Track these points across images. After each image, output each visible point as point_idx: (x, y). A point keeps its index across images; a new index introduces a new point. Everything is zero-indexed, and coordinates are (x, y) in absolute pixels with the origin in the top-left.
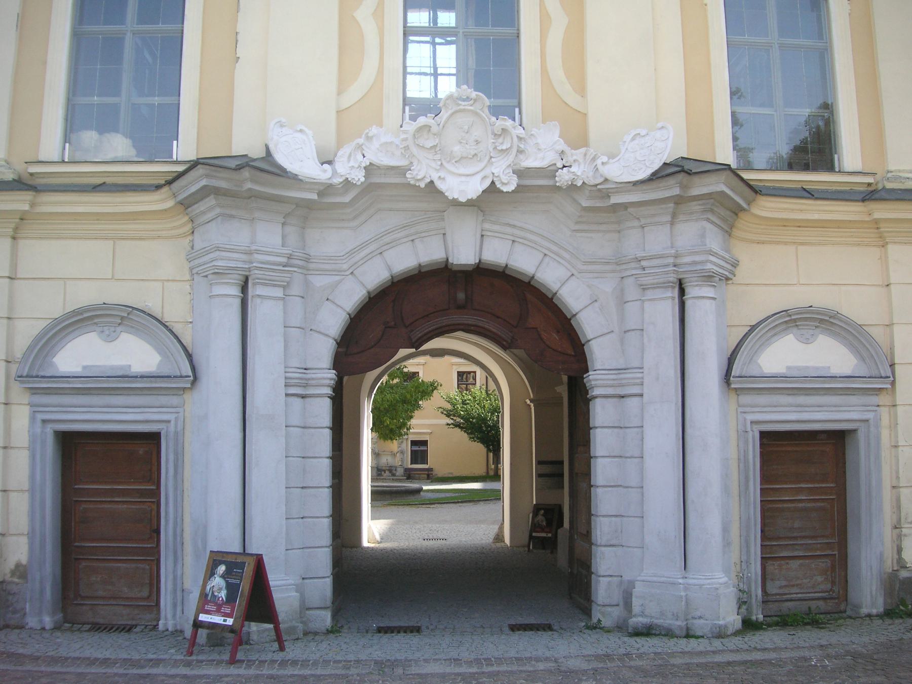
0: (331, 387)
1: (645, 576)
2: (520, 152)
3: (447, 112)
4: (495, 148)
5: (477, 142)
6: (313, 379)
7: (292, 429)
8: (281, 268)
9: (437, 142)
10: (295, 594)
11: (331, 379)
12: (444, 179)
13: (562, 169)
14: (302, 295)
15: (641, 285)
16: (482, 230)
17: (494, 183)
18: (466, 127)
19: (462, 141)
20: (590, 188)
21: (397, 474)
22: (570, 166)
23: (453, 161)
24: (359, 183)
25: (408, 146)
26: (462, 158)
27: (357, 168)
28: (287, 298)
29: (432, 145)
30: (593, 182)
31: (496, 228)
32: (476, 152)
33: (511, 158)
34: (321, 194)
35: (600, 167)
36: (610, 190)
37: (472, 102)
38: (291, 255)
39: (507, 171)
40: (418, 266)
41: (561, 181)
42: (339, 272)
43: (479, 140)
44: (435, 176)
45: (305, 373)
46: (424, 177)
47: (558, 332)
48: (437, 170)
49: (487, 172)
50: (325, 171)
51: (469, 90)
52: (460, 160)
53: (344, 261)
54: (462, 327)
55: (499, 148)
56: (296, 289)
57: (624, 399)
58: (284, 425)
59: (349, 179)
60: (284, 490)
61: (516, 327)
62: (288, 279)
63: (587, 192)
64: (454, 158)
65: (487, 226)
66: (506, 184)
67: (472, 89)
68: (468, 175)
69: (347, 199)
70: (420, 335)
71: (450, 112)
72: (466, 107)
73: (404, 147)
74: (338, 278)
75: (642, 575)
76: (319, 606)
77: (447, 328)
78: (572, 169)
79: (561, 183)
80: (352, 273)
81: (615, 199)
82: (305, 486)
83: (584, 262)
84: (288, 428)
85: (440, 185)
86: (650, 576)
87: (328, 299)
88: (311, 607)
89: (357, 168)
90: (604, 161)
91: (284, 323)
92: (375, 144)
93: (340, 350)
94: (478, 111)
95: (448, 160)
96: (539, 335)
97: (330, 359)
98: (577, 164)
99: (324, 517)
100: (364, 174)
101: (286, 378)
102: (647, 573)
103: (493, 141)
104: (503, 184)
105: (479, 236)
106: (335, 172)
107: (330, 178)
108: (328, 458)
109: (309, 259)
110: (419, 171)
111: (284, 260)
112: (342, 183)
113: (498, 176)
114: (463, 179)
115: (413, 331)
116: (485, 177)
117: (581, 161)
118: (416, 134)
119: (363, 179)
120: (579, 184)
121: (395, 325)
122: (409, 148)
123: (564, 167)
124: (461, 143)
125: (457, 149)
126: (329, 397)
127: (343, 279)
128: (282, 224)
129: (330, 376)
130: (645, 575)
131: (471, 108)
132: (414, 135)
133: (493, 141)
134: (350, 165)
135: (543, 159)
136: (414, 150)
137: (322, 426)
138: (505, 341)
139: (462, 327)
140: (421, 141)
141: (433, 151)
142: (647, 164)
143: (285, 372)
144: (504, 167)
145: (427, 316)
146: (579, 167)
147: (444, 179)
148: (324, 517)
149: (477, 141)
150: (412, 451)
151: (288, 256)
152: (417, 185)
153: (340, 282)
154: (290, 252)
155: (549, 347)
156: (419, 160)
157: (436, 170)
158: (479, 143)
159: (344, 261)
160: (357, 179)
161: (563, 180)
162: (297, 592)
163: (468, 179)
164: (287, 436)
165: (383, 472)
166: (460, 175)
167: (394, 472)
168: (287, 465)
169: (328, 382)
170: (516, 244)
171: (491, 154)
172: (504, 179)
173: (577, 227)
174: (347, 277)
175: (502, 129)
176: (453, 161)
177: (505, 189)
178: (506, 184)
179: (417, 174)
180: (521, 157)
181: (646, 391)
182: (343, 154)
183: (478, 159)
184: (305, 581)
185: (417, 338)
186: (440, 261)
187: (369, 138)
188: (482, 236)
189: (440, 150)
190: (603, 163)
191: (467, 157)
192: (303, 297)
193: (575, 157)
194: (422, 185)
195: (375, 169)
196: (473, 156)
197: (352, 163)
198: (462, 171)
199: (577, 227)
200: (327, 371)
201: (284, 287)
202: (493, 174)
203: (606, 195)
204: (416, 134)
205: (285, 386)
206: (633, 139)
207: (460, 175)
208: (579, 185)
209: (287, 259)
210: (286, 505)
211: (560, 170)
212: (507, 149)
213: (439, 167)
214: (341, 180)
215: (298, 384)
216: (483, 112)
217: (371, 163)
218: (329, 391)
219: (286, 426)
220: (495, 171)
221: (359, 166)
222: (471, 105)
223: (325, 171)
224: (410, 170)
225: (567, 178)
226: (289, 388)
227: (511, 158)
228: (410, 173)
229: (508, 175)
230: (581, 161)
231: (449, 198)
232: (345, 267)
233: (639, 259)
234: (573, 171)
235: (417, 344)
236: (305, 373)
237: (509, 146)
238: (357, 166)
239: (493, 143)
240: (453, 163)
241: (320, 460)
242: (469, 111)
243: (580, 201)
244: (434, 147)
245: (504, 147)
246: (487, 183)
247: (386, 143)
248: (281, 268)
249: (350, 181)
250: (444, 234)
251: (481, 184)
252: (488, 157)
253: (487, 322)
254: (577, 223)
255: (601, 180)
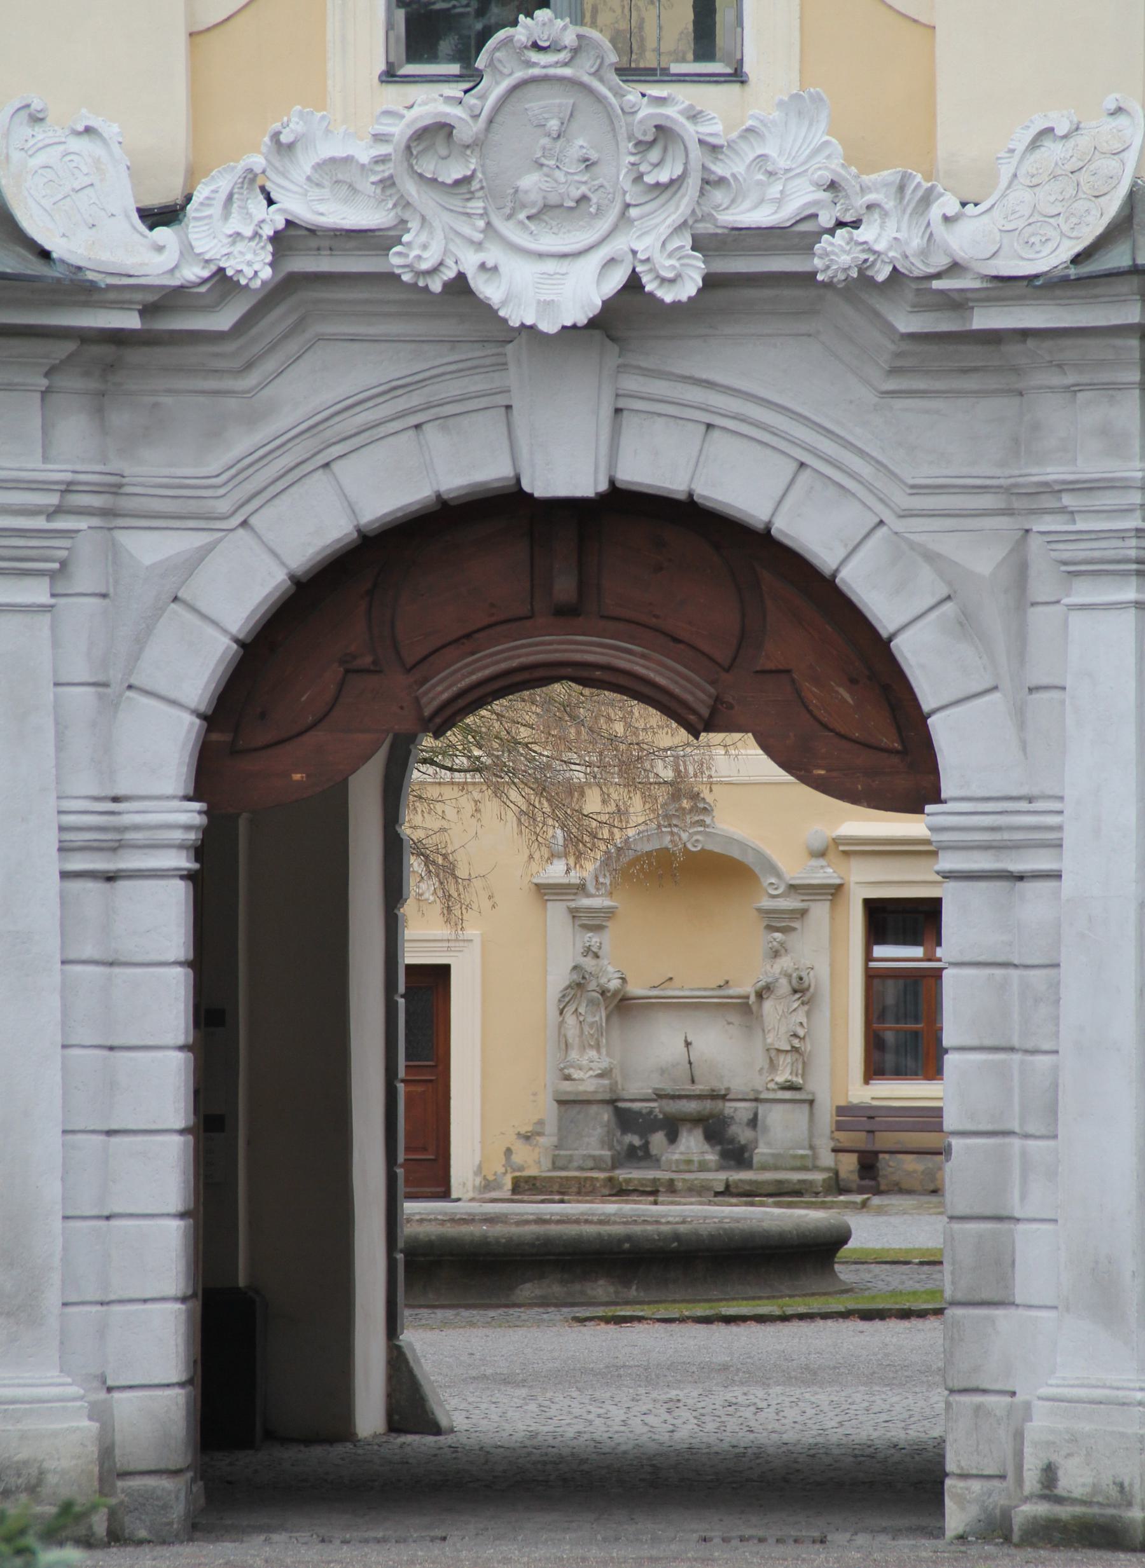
0: (187, 848)
1: (1058, 1386)
2: (710, 182)
3: (497, 83)
4: (639, 178)
5: (588, 164)
6: (137, 828)
7: (79, 968)
8: (40, 523)
9: (472, 167)
10: (86, 1423)
11: (188, 828)
12: (495, 269)
13: (831, 232)
14: (104, 591)
15: (1065, 563)
16: (617, 395)
17: (639, 279)
18: (553, 124)
19: (543, 161)
20: (914, 286)
21: (762, 1151)
22: (856, 224)
23: (522, 216)
24: (256, 284)
25: (391, 177)
26: (547, 208)
27: (251, 239)
28: (62, 601)
29: (459, 176)
30: (920, 268)
31: (659, 387)
32: (584, 189)
33: (680, 208)
34: (148, 311)
35: (938, 228)
36: (969, 295)
37: (563, 56)
38: (70, 483)
39: (676, 243)
40: (434, 498)
41: (828, 267)
42: (205, 519)
43: (594, 155)
44: (469, 262)
45: (112, 813)
46: (441, 264)
47: (853, 681)
48: (479, 246)
49: (620, 244)
50: (160, 249)
51: (559, 23)
52: (540, 212)
53: (222, 491)
54: (569, 671)
55: (649, 179)
56: (85, 578)
57: (1020, 885)
58: (57, 958)
59: (229, 272)
60: (57, 1139)
61: (727, 670)
62: (64, 554)
63: (910, 295)
64: (523, 206)
65: (631, 383)
66: (672, 281)
67: (568, 20)
68: (564, 256)
69: (223, 320)
70: (445, 696)
71: (505, 85)
72: (552, 71)
73: (381, 181)
74: (200, 539)
75: (1052, 1381)
76: (153, 1468)
77: (525, 676)
78: (861, 234)
79: (830, 273)
80: (244, 524)
81: (984, 319)
82: (115, 1127)
83: (913, 487)
84: (68, 967)
85: (489, 290)
86: (1072, 1386)
87: (175, 599)
88: (131, 1468)
89: (251, 239)
90: (950, 213)
91: (55, 671)
92: (305, 163)
93: (215, 737)
94: (586, 79)
95: (507, 211)
96: (798, 692)
97: (184, 769)
98: (876, 215)
99: (168, 1215)
100: (269, 258)
101: (62, 829)
102: (1064, 1378)
103: (632, 159)
104: (664, 281)
105: (606, 412)
106: (187, 250)
107: (172, 271)
108: (181, 1048)
109: (121, 486)
110: (425, 247)
111: (53, 499)
112: (205, 281)
113: (648, 260)
114: (551, 266)
115: (426, 680)
116: (612, 261)
117: (889, 205)
118: (413, 144)
119: (266, 273)
120: (882, 274)
121: (374, 663)
122: (394, 184)
123: (840, 224)
124: (542, 165)
125: (530, 181)
126: (182, 877)
127: (219, 541)
128: (42, 392)
129: (183, 818)
130: (1059, 1382)
131: (567, 72)
132: (408, 148)
133: (632, 159)
134: (230, 232)
135: (780, 202)
136: (411, 188)
137: (162, 958)
138: (694, 712)
139: (569, 671)
140: (427, 166)
141: (463, 189)
142: (1065, 228)
143: (60, 812)
144: (664, 230)
145: (468, 636)
146: (882, 227)
147: (495, 269)
148: (168, 1215)
149: (587, 160)
150: (873, 978)
151: (63, 487)
152: (421, 284)
153: (206, 551)
154: (69, 476)
155: (825, 727)
156: (423, 219)
157: (472, 242)
158: (593, 164)
159: (222, 491)
160: (250, 274)
161: (835, 267)
162: (90, 1418)
163: (563, 266)
164: (66, 990)
165: (658, 1139)
166: (541, 256)
167: (743, 1135)
168: (64, 1068)
169: (178, 835)
170: (716, 434)
171: (628, 199)
172: (666, 265)
173: (891, 385)
174: (231, 535)
175: (657, 127)
176: (522, 216)
177: (668, 296)
178: (672, 281)
179: (419, 257)
180: (718, 196)
181: (1067, 865)
182: (208, 198)
183: (593, 210)
184: (116, 1395)
185: (436, 704)
186: (496, 485)
187: (283, 148)
188: (618, 411)
189: (482, 188)
190: (946, 219)
191: (561, 206)
192: (104, 596)
193: (871, 197)
194: (436, 286)
195: (305, 236)
196: (578, 202)
197: (236, 224)
198: (549, 241)
199: (891, 385)
200: (176, 804)
201: (52, 575)
202: (634, 253)
203: (957, 303)
204: (413, 144)
205: (60, 850)
206: (1035, 143)
207: (541, 256)
208: (881, 277)
209: (58, 494)
210: (63, 1180)
211: (826, 237)
212: (672, 182)
213: (478, 237)
214: (206, 274)
215: (95, 844)
216: (601, 80)
217: (289, 223)
218: (184, 862)
219: (63, 962)
220: (638, 246)
221: (256, 235)
222: (566, 64)
223: (160, 249)
224: (400, 243)
225: (845, 259)
226: (70, 854)
227: (680, 208)
228: (399, 254)
229: (678, 254)
230: (889, 205)
231: (511, 323)
232: (224, 506)
233: (1057, 488)
234: (861, 239)
235: (438, 720)
236: (112, 813)
237: (678, 171)
238: (248, 232)
239: (633, 164)
240: (521, 223)
241: (159, 1054)
242: (561, 79)
243: (891, 318)
244: (465, 181)
245: (664, 177)
246: (616, 280)
247: (333, 160)
248: (40, 523)
249: (231, 278)
250: (508, 407)
251: (598, 282)
252: (617, 208)
253: (643, 656)
254: (894, 371)
255: (940, 262)
